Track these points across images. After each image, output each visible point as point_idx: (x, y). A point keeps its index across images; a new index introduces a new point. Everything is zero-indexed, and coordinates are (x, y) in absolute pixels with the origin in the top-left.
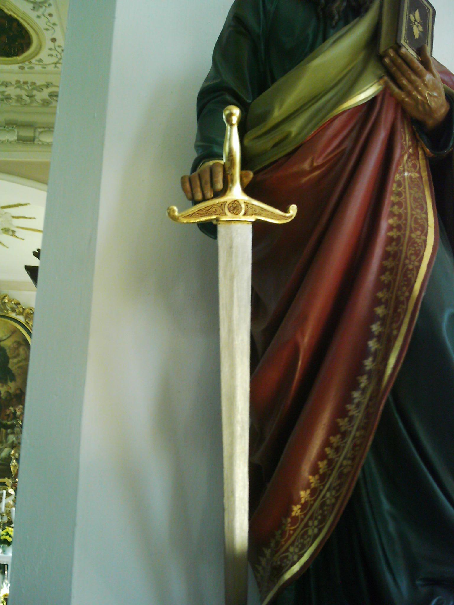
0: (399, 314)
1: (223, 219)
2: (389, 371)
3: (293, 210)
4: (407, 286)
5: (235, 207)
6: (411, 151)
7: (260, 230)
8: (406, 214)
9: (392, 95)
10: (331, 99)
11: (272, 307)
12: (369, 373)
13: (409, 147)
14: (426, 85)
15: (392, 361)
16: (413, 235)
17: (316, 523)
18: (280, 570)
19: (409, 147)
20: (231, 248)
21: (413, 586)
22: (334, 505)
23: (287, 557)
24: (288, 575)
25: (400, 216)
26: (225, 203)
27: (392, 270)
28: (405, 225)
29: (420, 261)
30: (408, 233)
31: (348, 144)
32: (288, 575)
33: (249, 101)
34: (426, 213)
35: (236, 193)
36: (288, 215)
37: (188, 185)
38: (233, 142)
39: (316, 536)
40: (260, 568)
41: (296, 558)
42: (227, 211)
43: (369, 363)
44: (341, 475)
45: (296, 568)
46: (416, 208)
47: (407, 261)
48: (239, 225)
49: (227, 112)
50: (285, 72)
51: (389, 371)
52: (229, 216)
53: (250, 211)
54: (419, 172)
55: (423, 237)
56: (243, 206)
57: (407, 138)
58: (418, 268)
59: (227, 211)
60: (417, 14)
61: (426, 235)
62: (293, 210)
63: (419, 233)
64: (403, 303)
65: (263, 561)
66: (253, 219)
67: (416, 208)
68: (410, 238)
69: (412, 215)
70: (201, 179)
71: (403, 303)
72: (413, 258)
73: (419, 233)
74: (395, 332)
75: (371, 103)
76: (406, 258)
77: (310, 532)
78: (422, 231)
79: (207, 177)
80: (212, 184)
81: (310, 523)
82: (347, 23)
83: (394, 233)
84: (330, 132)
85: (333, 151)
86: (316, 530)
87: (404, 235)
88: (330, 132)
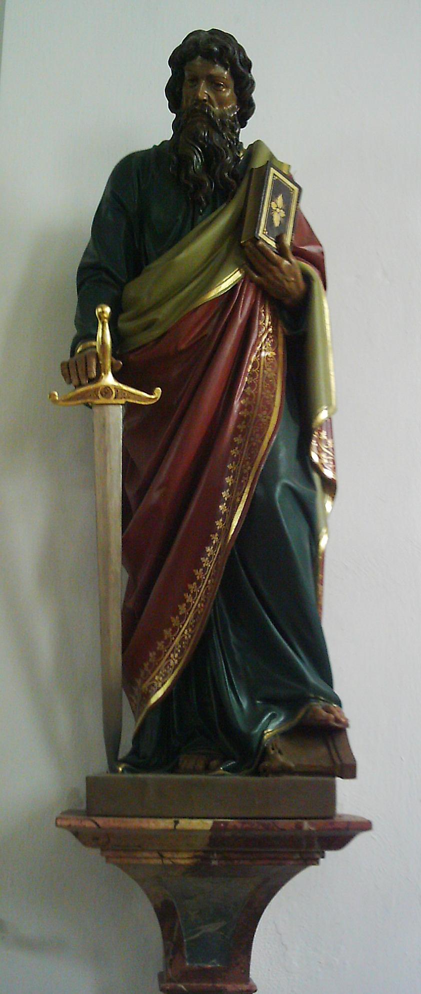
0: (242, 484)
1: (97, 402)
2: (232, 533)
3: (158, 391)
4: (250, 461)
5: (107, 391)
6: (270, 330)
7: (131, 409)
8: (257, 394)
9: (251, 281)
10: (195, 288)
11: (144, 468)
12: (220, 532)
13: (269, 327)
14: (282, 272)
15: (235, 523)
16: (260, 416)
17: (176, 655)
18: (148, 696)
19: (269, 327)
20: (104, 426)
21: (252, 703)
22: (190, 640)
23: (153, 685)
24: (154, 700)
25: (251, 397)
26: (97, 389)
27: (240, 447)
28: (255, 405)
29: (262, 440)
30: (256, 412)
31: (209, 331)
32: (154, 700)
33: (124, 280)
34: (275, 394)
35: (109, 380)
36: (153, 397)
37: (66, 371)
38: (104, 334)
39: (176, 666)
40: (133, 698)
41: (160, 684)
42: (100, 395)
43: (219, 524)
44: (196, 616)
45: (160, 694)
46: (267, 388)
47: (252, 439)
48: (110, 407)
49: (100, 310)
50: (159, 255)
51: (232, 533)
52: (102, 400)
53: (120, 395)
54: (276, 351)
55: (268, 417)
56: (114, 391)
57: (267, 318)
58: (260, 445)
59: (100, 395)
60: (280, 199)
61: (270, 415)
62: (158, 391)
63: (265, 413)
64: (245, 475)
65: (136, 690)
66: (123, 401)
67: (267, 388)
68: (257, 418)
69: (262, 395)
70: (78, 370)
71: (245, 475)
72: (257, 436)
73: (265, 413)
74: (238, 500)
75: (234, 288)
76: (252, 436)
77: (172, 663)
78: (268, 411)
79: (81, 367)
80: (87, 373)
81: (172, 656)
82: (214, 209)
83: (244, 413)
84: (193, 320)
85: (195, 337)
86: (176, 661)
87: (253, 415)
88: (193, 320)
